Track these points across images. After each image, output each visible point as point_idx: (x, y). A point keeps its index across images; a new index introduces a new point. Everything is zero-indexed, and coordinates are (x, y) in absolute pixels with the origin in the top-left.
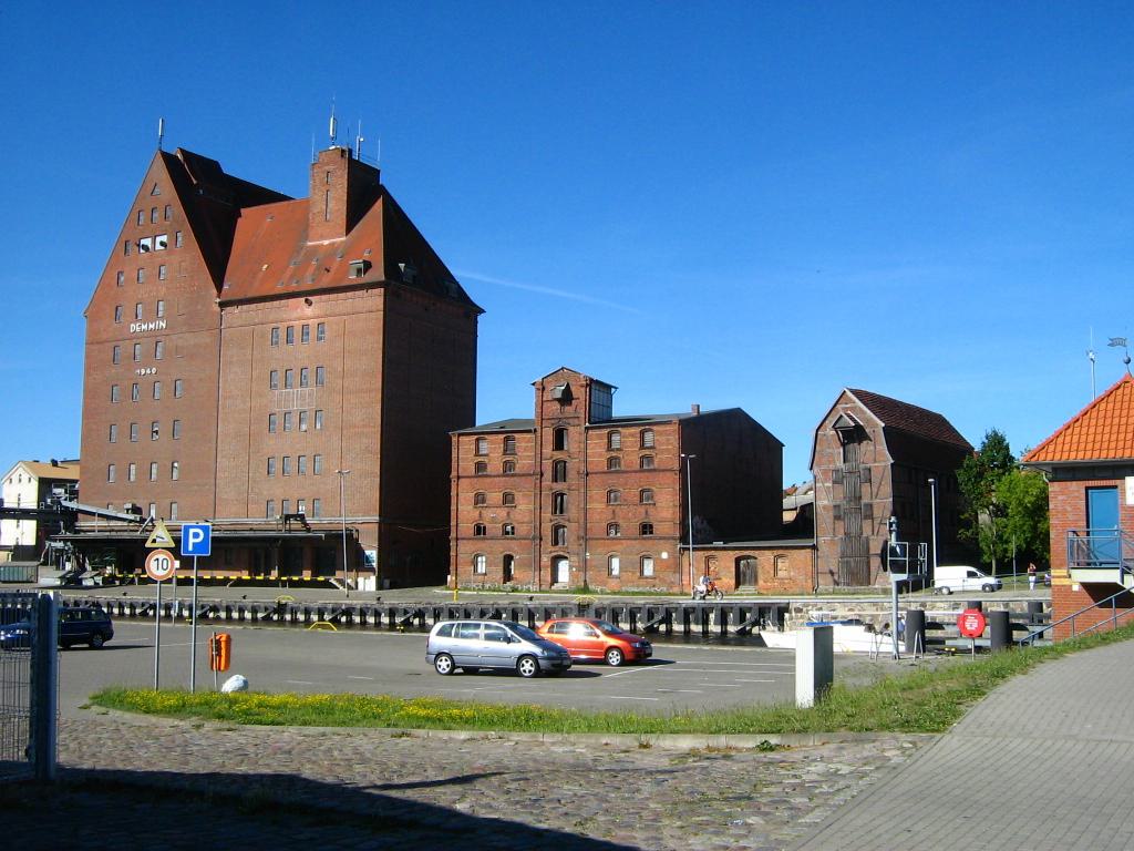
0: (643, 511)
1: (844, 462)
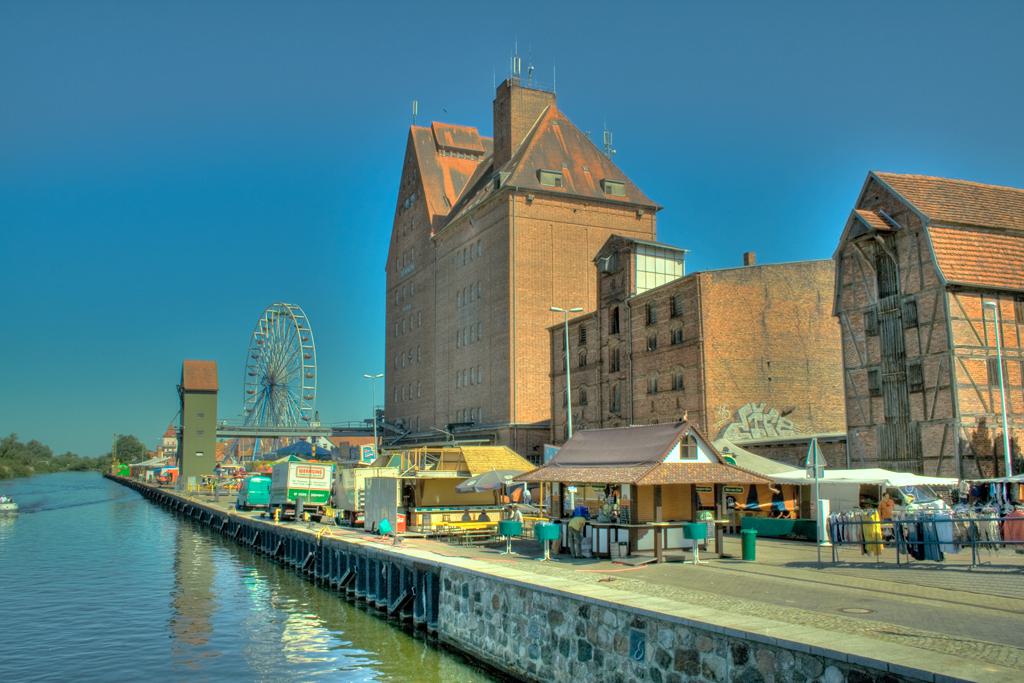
0: (675, 400)
1: (882, 295)
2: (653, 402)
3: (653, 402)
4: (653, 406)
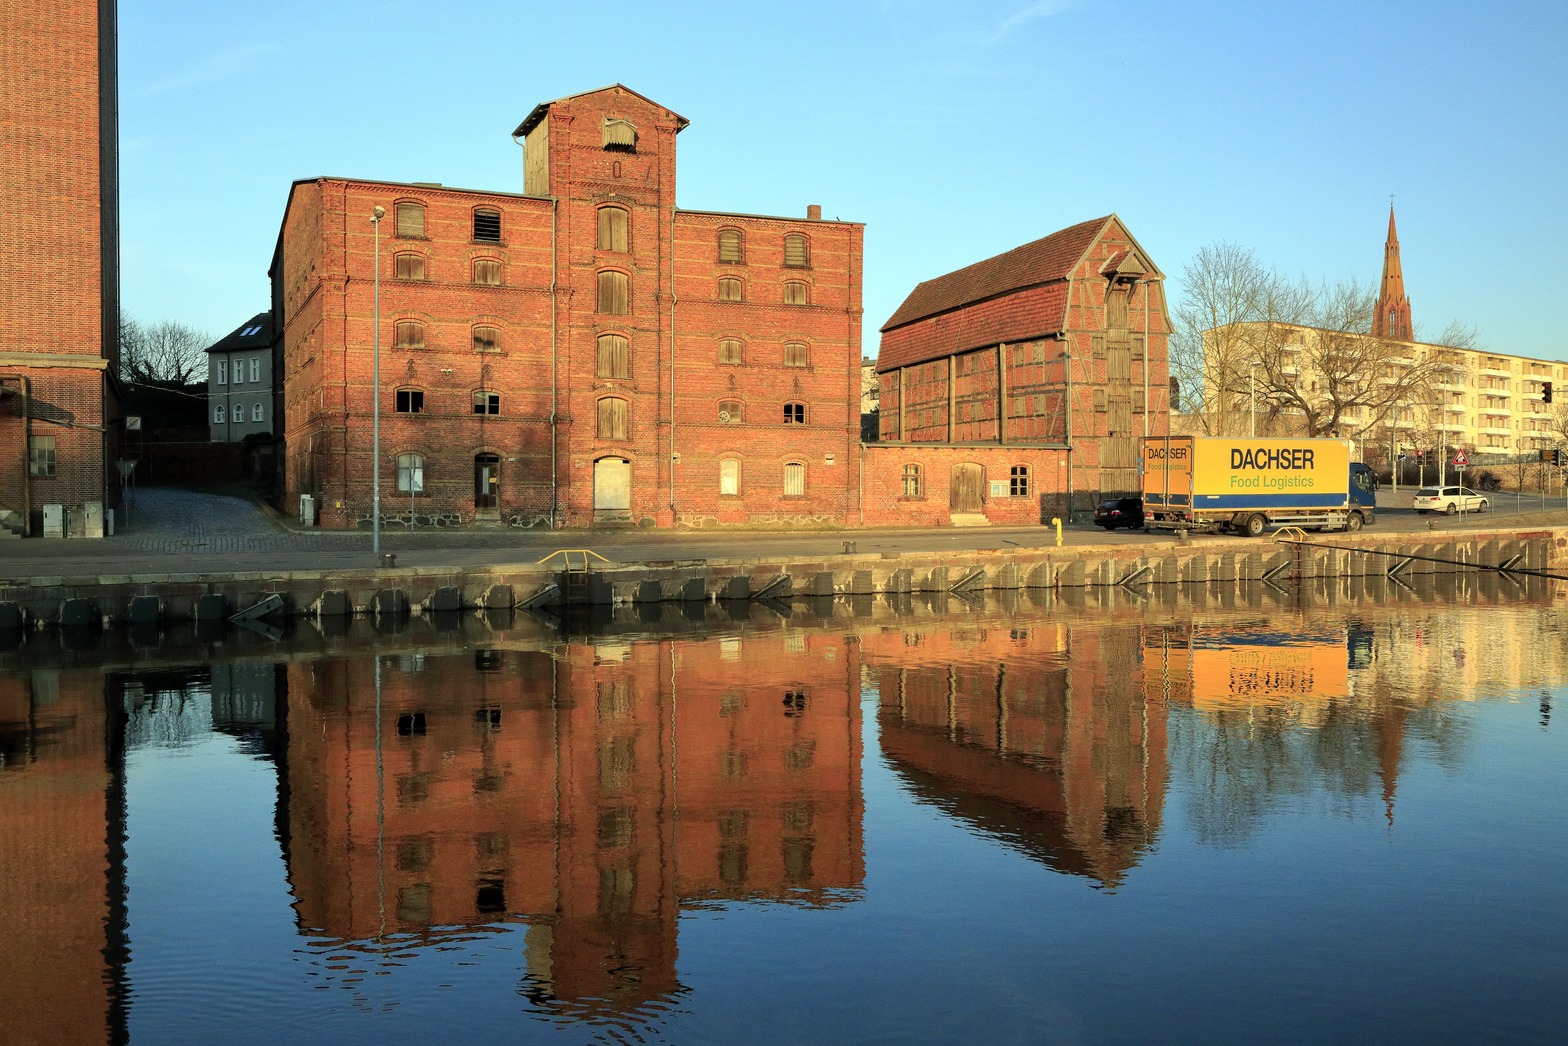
2: (732, 377)
3: (732, 377)
4: (732, 383)
